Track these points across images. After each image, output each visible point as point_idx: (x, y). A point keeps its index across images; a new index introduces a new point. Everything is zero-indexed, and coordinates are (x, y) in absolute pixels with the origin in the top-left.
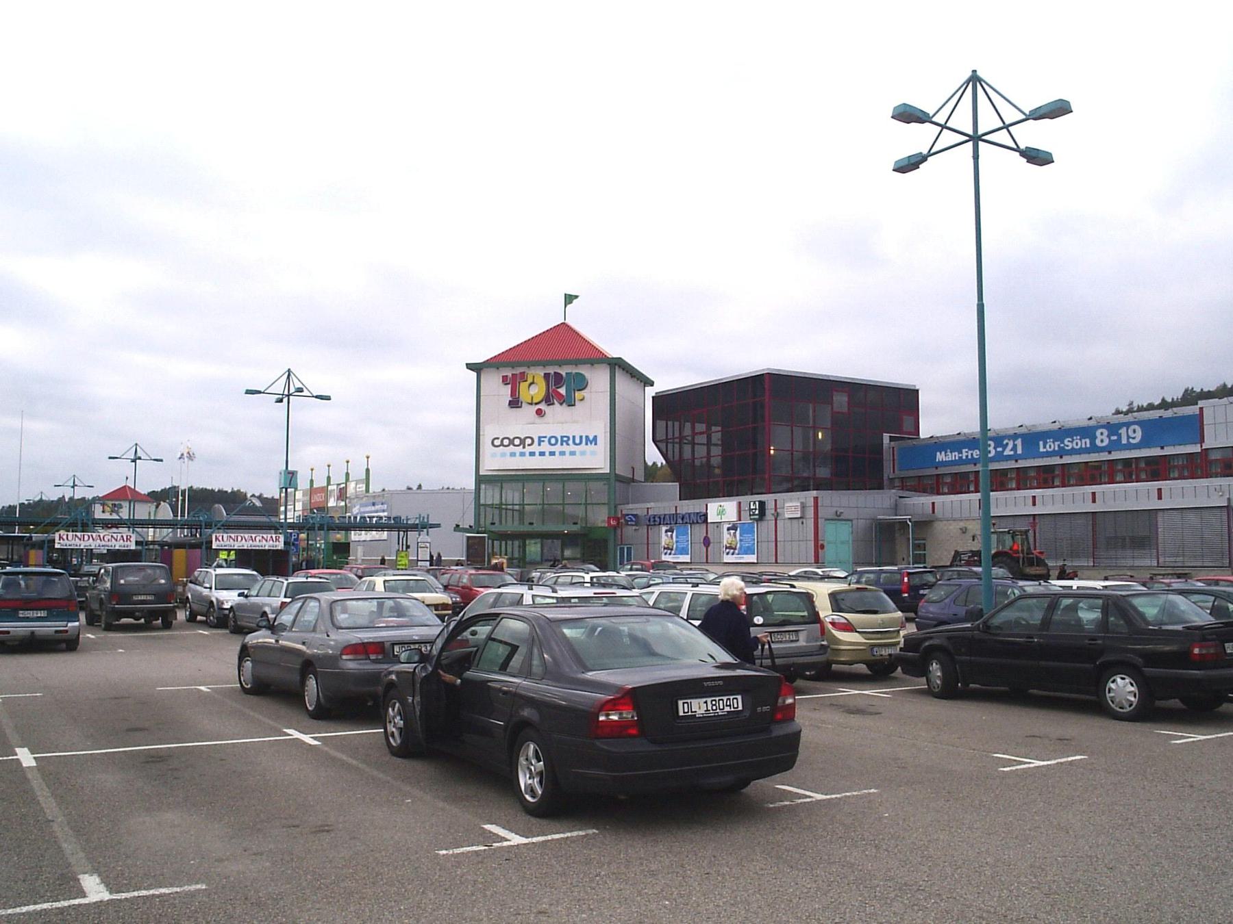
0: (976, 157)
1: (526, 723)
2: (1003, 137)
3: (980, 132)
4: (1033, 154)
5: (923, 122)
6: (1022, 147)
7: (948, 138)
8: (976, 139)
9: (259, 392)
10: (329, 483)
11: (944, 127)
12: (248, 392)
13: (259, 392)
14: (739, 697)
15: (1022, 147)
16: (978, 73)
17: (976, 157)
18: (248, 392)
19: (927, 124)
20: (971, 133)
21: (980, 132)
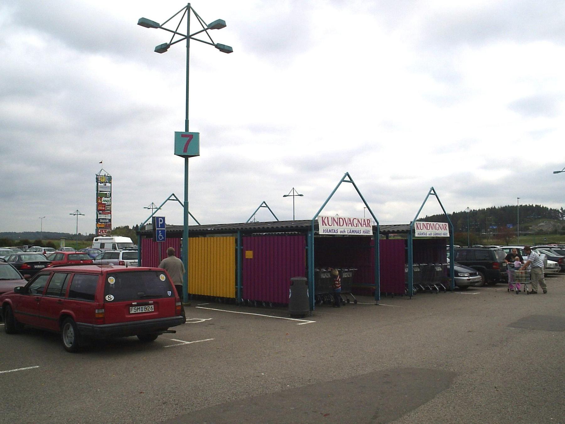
0: (188, 46)
1: (67, 315)
2: (203, 36)
3: (190, 34)
4: (222, 47)
5: (157, 28)
6: (216, 43)
7: (177, 37)
8: (188, 37)
9: (560, 172)
10: (104, 226)
11: (175, 33)
12: (555, 173)
13: (560, 172)
14: (447, 224)
15: (216, 43)
16: (192, 6)
17: (188, 46)
18: (555, 173)
19: (159, 29)
20: (186, 34)
21: (190, 34)
